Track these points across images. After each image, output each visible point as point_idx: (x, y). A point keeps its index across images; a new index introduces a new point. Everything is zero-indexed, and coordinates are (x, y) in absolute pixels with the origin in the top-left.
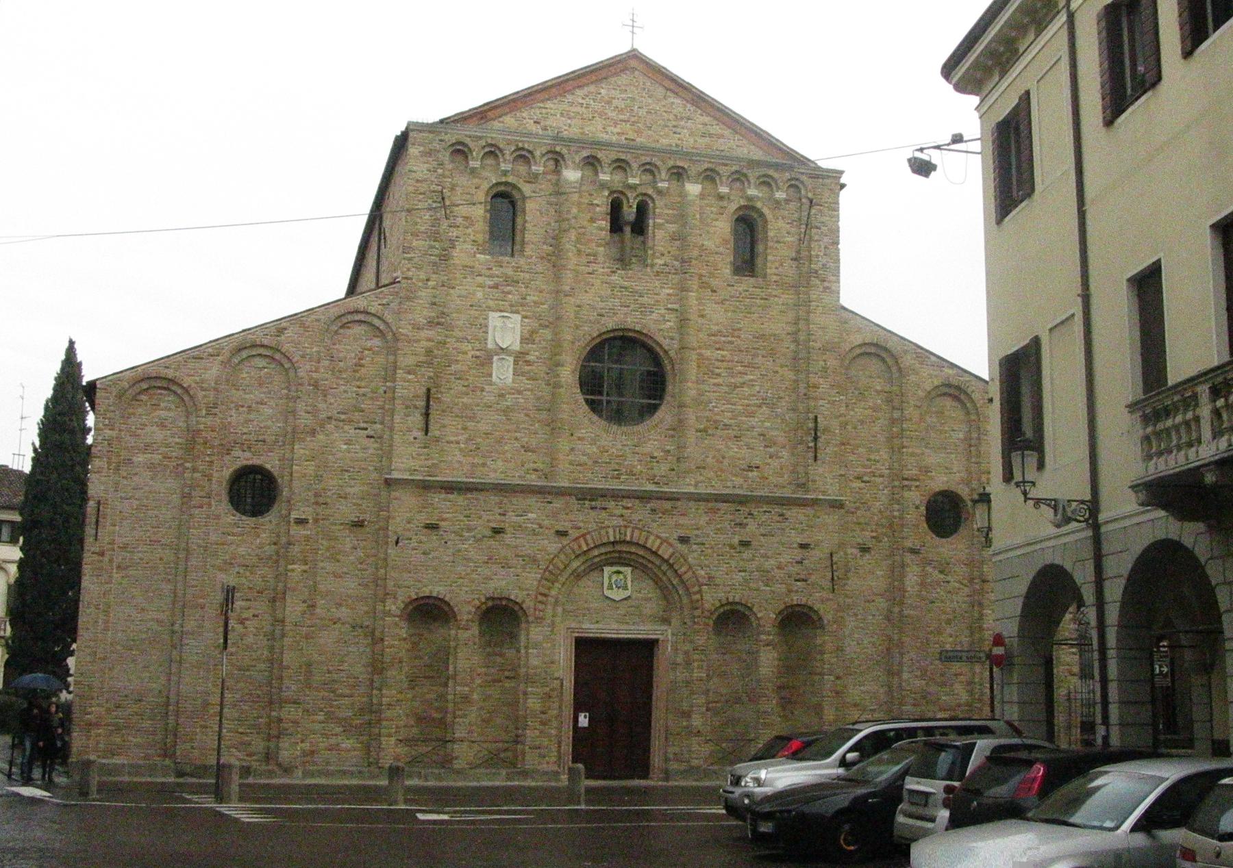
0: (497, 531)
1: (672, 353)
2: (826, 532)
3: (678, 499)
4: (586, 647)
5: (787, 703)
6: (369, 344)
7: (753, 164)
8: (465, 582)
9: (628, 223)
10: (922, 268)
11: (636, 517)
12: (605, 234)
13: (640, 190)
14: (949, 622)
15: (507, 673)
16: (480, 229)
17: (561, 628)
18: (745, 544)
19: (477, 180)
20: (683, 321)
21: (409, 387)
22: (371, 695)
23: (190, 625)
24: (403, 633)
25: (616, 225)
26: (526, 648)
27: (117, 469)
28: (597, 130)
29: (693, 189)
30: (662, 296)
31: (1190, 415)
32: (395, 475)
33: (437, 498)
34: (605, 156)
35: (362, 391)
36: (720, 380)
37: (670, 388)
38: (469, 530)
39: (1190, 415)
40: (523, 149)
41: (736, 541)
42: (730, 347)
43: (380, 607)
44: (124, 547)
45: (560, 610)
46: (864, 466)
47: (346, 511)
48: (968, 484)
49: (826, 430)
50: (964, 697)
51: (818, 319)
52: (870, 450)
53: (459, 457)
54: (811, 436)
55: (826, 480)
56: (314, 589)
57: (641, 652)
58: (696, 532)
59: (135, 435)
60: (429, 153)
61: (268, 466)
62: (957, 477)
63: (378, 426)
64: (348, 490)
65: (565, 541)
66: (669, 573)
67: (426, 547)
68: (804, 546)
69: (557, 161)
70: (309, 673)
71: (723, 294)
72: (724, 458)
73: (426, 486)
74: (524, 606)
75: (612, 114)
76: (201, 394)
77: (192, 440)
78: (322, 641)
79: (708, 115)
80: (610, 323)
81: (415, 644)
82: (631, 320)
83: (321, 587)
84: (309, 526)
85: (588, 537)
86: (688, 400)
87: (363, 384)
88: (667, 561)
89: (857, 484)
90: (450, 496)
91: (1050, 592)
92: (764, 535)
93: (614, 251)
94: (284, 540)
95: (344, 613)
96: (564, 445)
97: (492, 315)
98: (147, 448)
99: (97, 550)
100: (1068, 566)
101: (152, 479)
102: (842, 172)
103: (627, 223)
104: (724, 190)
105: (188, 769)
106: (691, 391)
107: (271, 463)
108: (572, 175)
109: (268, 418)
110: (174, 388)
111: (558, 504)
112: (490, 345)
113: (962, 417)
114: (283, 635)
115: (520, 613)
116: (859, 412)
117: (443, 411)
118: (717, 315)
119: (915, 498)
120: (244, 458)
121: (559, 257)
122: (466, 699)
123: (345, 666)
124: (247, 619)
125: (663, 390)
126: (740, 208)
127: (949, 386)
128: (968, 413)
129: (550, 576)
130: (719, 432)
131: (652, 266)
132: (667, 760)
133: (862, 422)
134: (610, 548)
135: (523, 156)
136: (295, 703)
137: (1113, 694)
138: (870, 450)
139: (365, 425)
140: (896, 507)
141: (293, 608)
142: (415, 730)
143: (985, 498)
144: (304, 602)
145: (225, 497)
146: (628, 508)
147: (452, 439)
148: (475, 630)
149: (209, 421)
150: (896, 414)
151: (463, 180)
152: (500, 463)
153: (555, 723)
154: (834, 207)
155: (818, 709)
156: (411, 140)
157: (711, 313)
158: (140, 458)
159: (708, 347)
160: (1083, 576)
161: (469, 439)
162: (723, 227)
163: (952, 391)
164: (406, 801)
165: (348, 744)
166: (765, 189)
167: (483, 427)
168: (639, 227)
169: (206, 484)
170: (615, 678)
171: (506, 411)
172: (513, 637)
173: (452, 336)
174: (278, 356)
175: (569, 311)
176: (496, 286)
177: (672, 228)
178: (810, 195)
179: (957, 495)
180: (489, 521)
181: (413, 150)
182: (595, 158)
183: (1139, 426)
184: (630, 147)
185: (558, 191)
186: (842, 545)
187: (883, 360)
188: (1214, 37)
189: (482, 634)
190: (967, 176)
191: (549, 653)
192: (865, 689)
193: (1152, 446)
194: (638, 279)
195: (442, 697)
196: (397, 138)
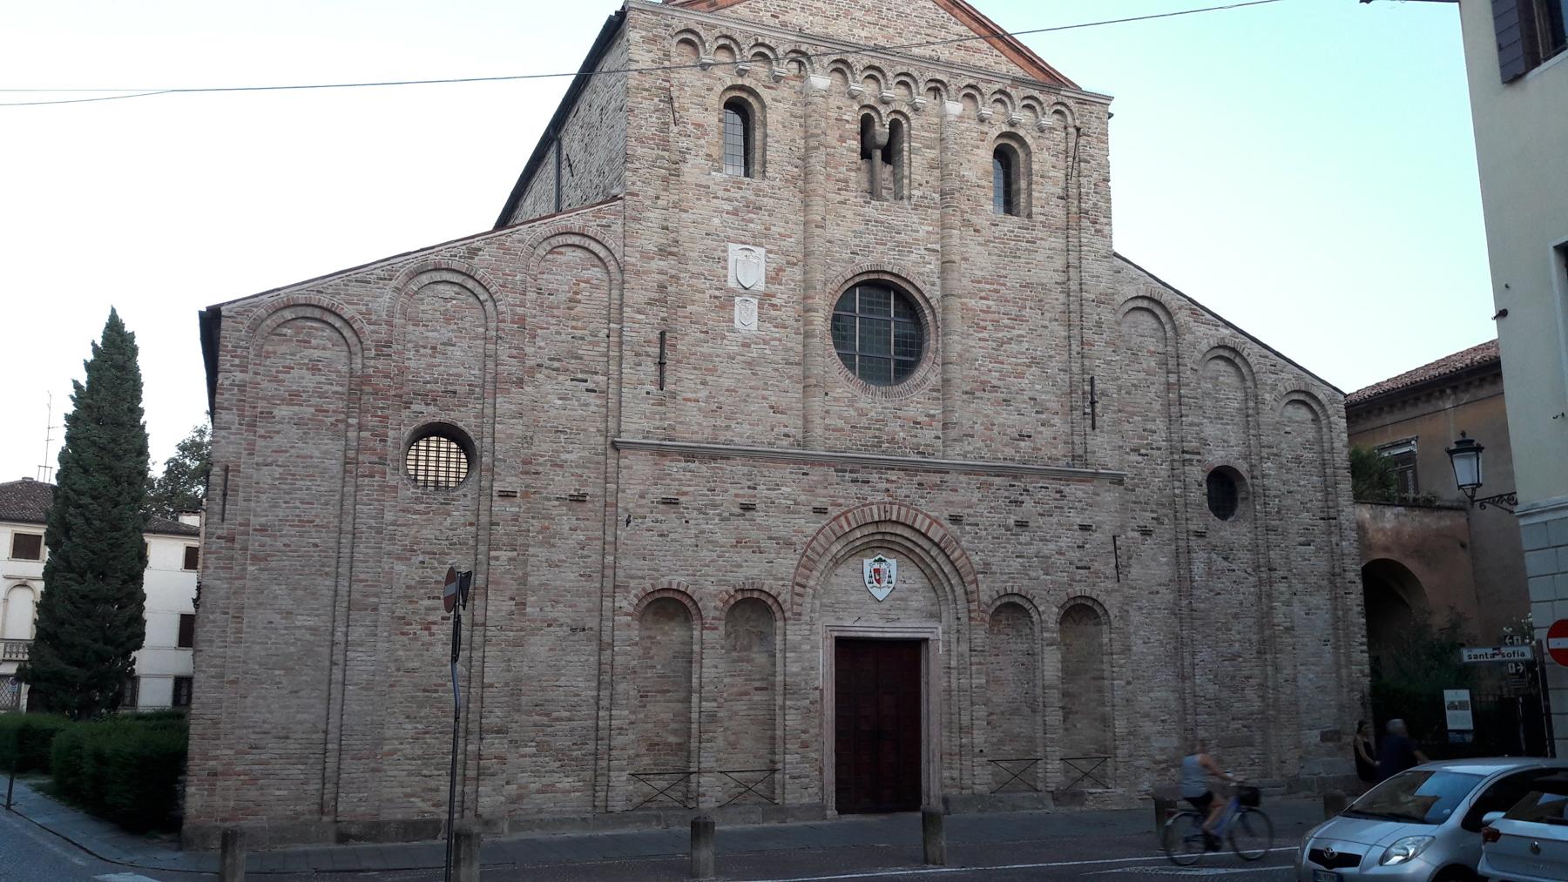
0: (747, 508)
1: (933, 302)
4: (849, 649)
7: (1017, 81)
8: (710, 567)
9: (881, 147)
11: (902, 492)
12: (856, 156)
13: (893, 107)
15: (758, 684)
16: (711, 143)
17: (819, 626)
18: (1022, 525)
19: (707, 81)
20: (946, 264)
21: (641, 328)
22: (597, 718)
23: (357, 633)
26: (784, 651)
27: (252, 425)
29: (954, 108)
32: (625, 437)
33: (676, 467)
34: (859, 61)
35: (578, 333)
36: (985, 335)
37: (931, 343)
38: (715, 506)
40: (763, 45)
41: (1011, 522)
42: (995, 296)
44: (263, 529)
45: (817, 603)
46: (1141, 438)
47: (563, 484)
48: (1246, 457)
50: (1257, 704)
51: (1092, 266)
52: (1146, 419)
53: (701, 419)
54: (1087, 401)
55: (1104, 449)
56: (523, 582)
57: (909, 652)
58: (971, 511)
59: (275, 380)
60: (653, 40)
61: (460, 424)
63: (601, 378)
64: (564, 456)
69: (800, 63)
71: (988, 233)
73: (661, 451)
74: (780, 599)
75: (858, 14)
76: (368, 328)
77: (357, 389)
78: (533, 649)
79: (964, 24)
80: (866, 263)
83: (533, 580)
84: (517, 500)
85: (850, 515)
87: (580, 324)
88: (937, 545)
89: (1134, 457)
90: (692, 465)
93: (863, 178)
95: (561, 613)
96: (817, 403)
97: (732, 247)
98: (294, 397)
99: (224, 533)
101: (301, 439)
102: (1110, 98)
103: (878, 147)
105: (354, 830)
106: (956, 346)
108: (820, 81)
109: (461, 362)
110: (331, 319)
111: (816, 474)
112: (732, 284)
113: (1238, 384)
114: (486, 641)
115: (775, 608)
116: (1134, 376)
117: (679, 362)
119: (1197, 473)
121: (806, 181)
122: (713, 717)
123: (563, 681)
124: (434, 623)
126: (1002, 135)
127: (1225, 347)
128: (1243, 379)
129: (807, 563)
131: (910, 198)
134: (872, 529)
136: (498, 732)
138: (1146, 419)
139: (584, 376)
140: (1177, 484)
142: (646, 760)
144: (512, 599)
147: (690, 395)
149: (381, 364)
150: (1173, 378)
151: (691, 77)
153: (815, 745)
154: (1103, 138)
157: (977, 259)
158: (282, 412)
159: (971, 295)
161: (710, 396)
162: (985, 156)
163: (1226, 354)
165: (566, 783)
167: (726, 382)
168: (890, 153)
169: (378, 445)
170: (880, 676)
171: (750, 364)
172: (765, 638)
173: (687, 271)
174: (470, 284)
175: (818, 246)
176: (735, 213)
177: (931, 154)
178: (1078, 123)
179: (1236, 471)
180: (736, 495)
181: (633, 35)
182: (844, 62)
185: (805, 98)
186: (1122, 527)
187: (1156, 317)
196: (610, 21)
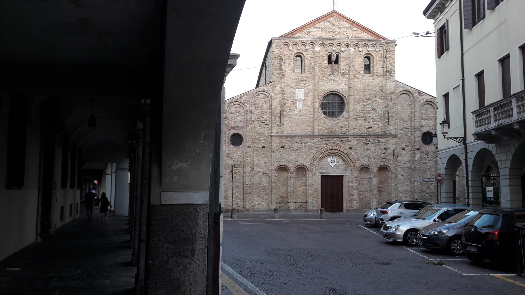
0: (300, 148)
2: (391, 144)
4: (324, 178)
5: (380, 192)
6: (264, 100)
7: (369, 41)
9: (333, 60)
10: (418, 68)
11: (337, 143)
12: (327, 65)
14: (429, 169)
21: (276, 110)
24: (276, 175)
25: (330, 62)
28: (324, 35)
29: (352, 50)
30: (344, 81)
31: (488, 115)
33: (284, 140)
34: (327, 42)
36: (360, 104)
37: (346, 107)
38: (292, 148)
39: (488, 115)
41: (365, 148)
43: (270, 168)
47: (261, 144)
49: (391, 116)
51: (389, 84)
54: (387, 118)
55: (391, 130)
56: (253, 164)
57: (339, 179)
60: (278, 46)
62: (431, 128)
65: (318, 150)
66: (347, 157)
67: (281, 152)
68: (385, 149)
70: (253, 186)
71: (361, 79)
75: (328, 30)
80: (329, 90)
81: (279, 178)
83: (255, 164)
86: (351, 110)
89: (401, 131)
91: (454, 162)
94: (245, 152)
95: (260, 170)
100: (458, 155)
104: (361, 49)
107: (241, 132)
109: (240, 120)
111: (316, 140)
112: (296, 98)
118: (359, 86)
119: (418, 134)
120: (235, 131)
125: (344, 107)
129: (314, 159)
132: (347, 207)
135: (304, 44)
137: (470, 191)
141: (248, 169)
143: (436, 135)
145: (230, 142)
148: (295, 173)
150: (413, 110)
155: (390, 194)
156: (273, 43)
159: (356, 95)
160: (462, 158)
163: (430, 103)
164: (279, 218)
165: (263, 203)
166: (373, 48)
167: (295, 120)
168: (337, 62)
170: (332, 186)
172: (305, 175)
174: (241, 104)
175: (317, 88)
177: (346, 62)
181: (273, 45)
183: (475, 118)
184: (334, 39)
188: (501, 4)
189: (296, 175)
190: (432, 43)
191: (315, 180)
192: (405, 187)
193: (479, 123)
194: (336, 77)
195: (287, 191)
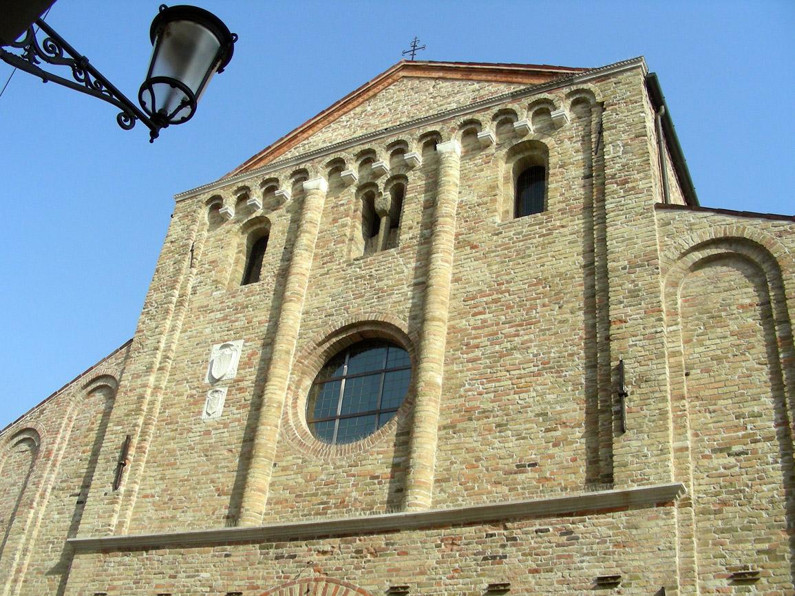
3: (397, 530)
7: (515, 96)
11: (333, 564)
52: (741, 400)
72: (478, 459)
82: (364, 311)
89: (721, 460)
90: (126, 559)
92: (534, 571)
130: (474, 424)
133: (718, 359)
138: (741, 400)
146: (324, 553)
152: (190, 513)
167: (182, 473)
176: (224, 319)
